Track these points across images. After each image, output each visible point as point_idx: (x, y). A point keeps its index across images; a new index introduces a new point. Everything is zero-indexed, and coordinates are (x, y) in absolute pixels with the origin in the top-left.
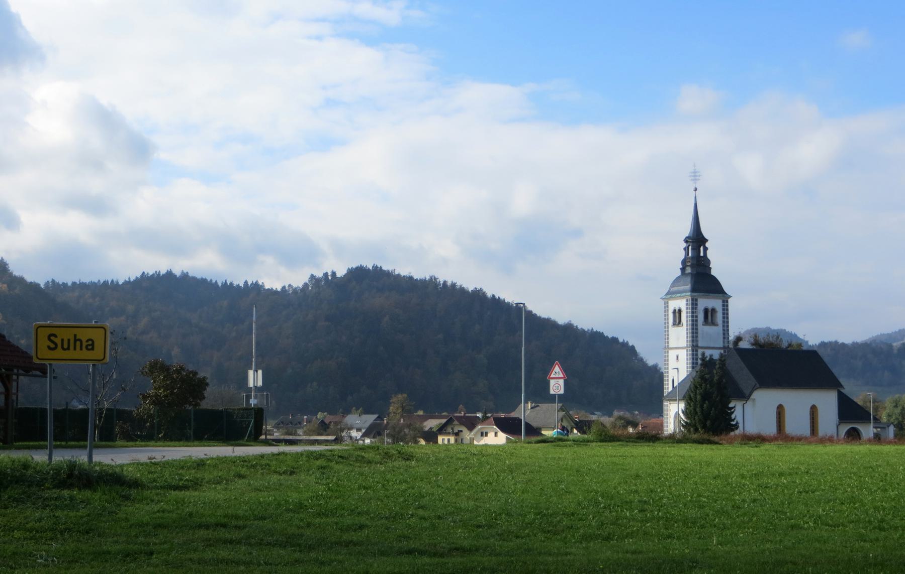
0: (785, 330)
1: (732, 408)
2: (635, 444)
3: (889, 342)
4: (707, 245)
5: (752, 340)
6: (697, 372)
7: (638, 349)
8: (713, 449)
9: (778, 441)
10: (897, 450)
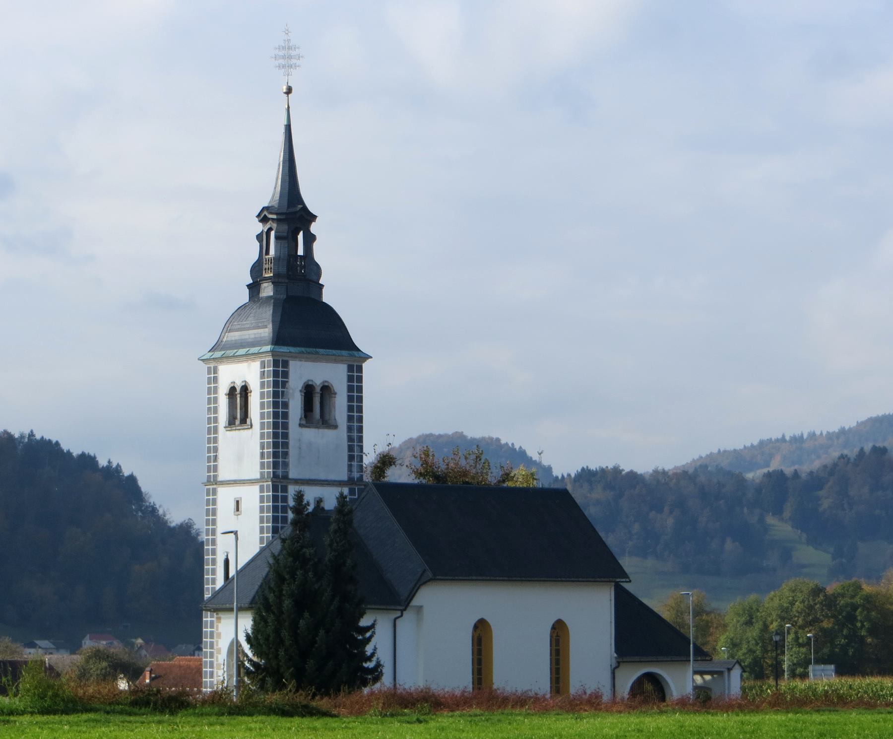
0: (498, 440)
1: (367, 629)
2: (128, 718)
3: (737, 472)
4: (314, 228)
5: (418, 464)
6: (284, 541)
7: (145, 485)
8: (315, 729)
9: (471, 706)
10: (743, 723)
